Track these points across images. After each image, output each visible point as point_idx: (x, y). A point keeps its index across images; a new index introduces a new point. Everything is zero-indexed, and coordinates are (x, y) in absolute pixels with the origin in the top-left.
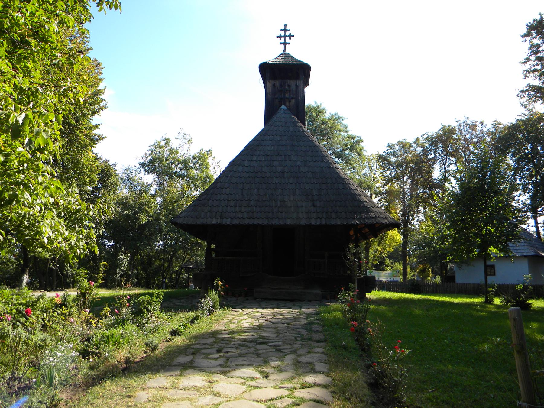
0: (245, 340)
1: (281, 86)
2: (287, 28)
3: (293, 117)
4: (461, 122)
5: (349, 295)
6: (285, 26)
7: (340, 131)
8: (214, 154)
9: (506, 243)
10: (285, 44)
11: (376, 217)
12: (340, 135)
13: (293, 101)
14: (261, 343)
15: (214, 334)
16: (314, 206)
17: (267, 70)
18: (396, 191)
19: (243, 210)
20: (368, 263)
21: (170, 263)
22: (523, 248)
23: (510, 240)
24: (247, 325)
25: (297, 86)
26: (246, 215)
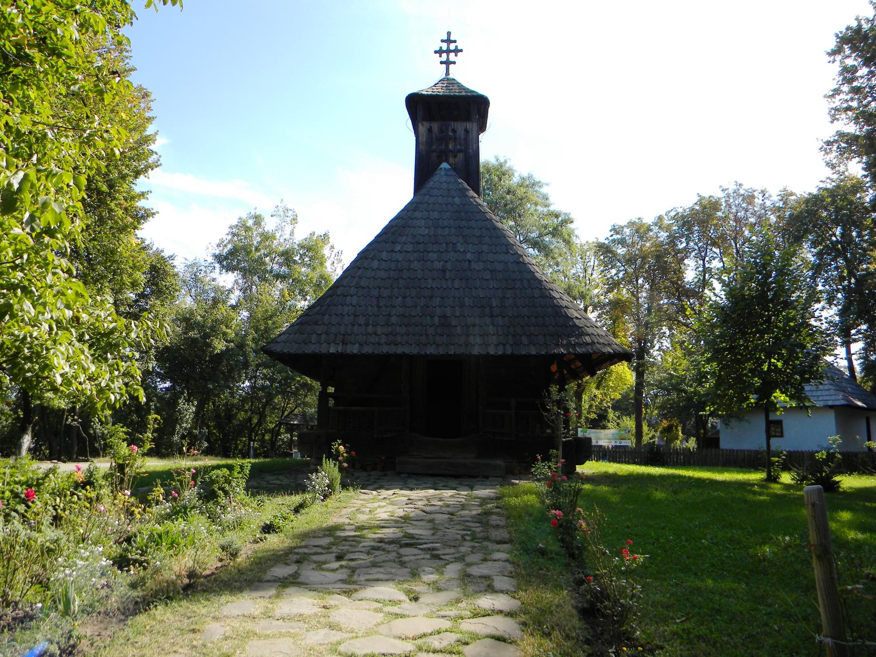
0: (381, 541)
1: (441, 131)
2: (452, 38)
3: (460, 181)
4: (731, 191)
5: (549, 467)
6: (449, 34)
7: (536, 204)
8: (332, 241)
10: (448, 63)
11: (593, 343)
12: (536, 210)
13: (461, 156)
14: (407, 545)
15: (331, 531)
17: (419, 106)
19: (379, 330)
20: (579, 417)
22: (827, 393)
24: (385, 516)
25: (467, 131)
26: (384, 339)
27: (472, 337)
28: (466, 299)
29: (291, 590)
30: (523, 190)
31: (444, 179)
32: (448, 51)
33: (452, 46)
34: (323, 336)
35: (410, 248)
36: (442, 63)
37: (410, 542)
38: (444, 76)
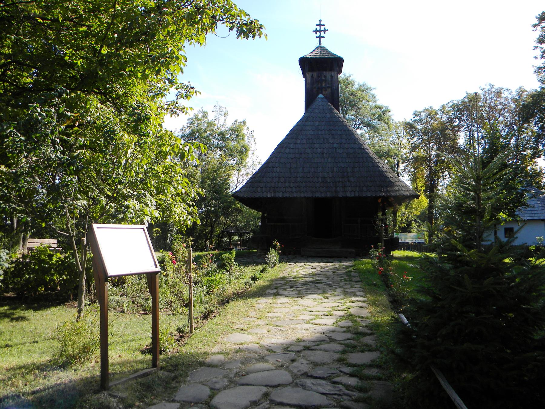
0: (306, 282)
1: (318, 77)
2: (322, 23)
3: (329, 104)
4: (487, 90)
5: (378, 251)
6: (320, 21)
7: (368, 101)
8: (248, 125)
9: (513, 209)
10: (320, 37)
11: (399, 190)
12: (368, 105)
13: (329, 90)
14: (318, 283)
15: (283, 278)
16: (349, 181)
17: (306, 64)
18: (423, 157)
19: (292, 185)
20: (395, 225)
21: (213, 228)
22: (540, 212)
23: (517, 207)
24: (304, 273)
25: (332, 77)
26: (294, 190)
27: (338, 188)
28: (335, 168)
29: (277, 297)
30: (361, 93)
31: (321, 103)
32: (320, 31)
33: (322, 28)
34: (264, 188)
35: (304, 141)
36: (317, 37)
37: (319, 282)
38: (318, 45)
